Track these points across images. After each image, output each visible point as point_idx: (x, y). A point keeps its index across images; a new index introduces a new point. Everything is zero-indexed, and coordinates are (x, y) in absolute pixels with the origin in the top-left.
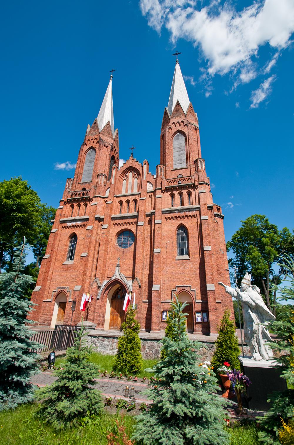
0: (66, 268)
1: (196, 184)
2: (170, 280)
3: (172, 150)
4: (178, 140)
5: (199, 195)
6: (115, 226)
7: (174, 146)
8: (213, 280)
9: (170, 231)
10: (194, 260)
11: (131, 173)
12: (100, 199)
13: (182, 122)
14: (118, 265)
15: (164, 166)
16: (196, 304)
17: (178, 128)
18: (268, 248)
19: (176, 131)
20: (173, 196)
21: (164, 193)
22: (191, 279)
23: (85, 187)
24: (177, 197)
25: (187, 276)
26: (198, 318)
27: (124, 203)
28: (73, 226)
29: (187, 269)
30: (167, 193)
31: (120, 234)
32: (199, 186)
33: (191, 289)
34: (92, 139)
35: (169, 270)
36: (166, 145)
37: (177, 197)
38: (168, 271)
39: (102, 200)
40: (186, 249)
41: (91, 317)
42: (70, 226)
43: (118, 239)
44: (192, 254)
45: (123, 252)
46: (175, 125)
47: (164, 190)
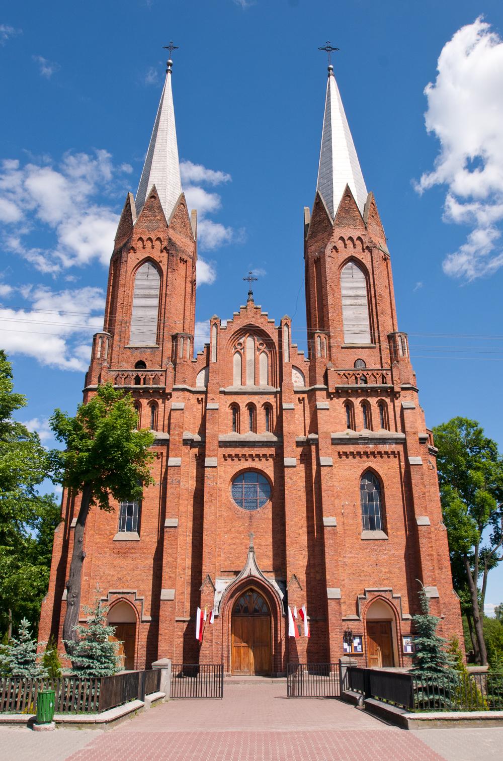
0: (124, 550)
1: (397, 389)
2: (354, 579)
4: (351, 280)
6: (226, 460)
8: (434, 580)
9: (347, 480)
10: (396, 540)
11: (249, 338)
12: (187, 394)
13: (359, 238)
14: (251, 549)
15: (327, 337)
16: (402, 623)
17: (351, 251)
18: (481, 493)
19: (347, 257)
20: (349, 406)
21: (332, 399)
22: (391, 576)
23: (144, 360)
25: (384, 570)
26: (406, 647)
27: (244, 410)
29: (384, 558)
30: (338, 398)
31: (238, 478)
32: (403, 393)
33: (394, 596)
34: (150, 239)
35: (350, 558)
36: (328, 287)
38: (348, 561)
40: (377, 516)
41: (208, 652)
43: (233, 488)
44: (392, 528)
45: (251, 518)
46: (345, 245)
47: (333, 393)
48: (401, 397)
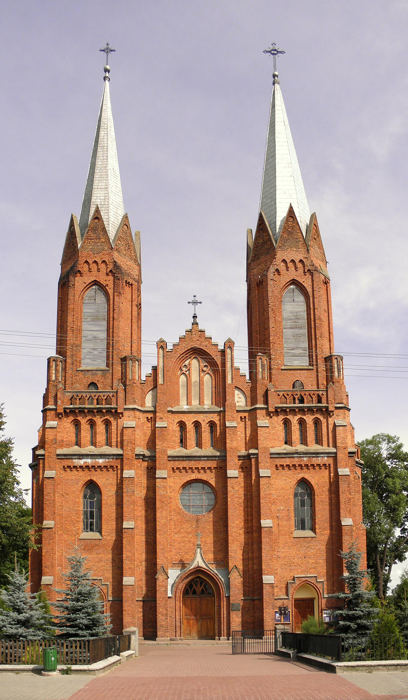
1: (331, 408)
3: (281, 322)
5: (122, 430)
7: (285, 315)
9: (283, 489)
12: (137, 413)
14: (199, 546)
20: (77, 424)
21: (271, 417)
22: (317, 565)
24: (85, 427)
25: (311, 561)
27: (190, 427)
28: (87, 467)
32: (336, 412)
33: (318, 580)
35: (283, 553)
37: (85, 427)
39: (141, 415)
42: (81, 467)
44: (320, 528)
47: (272, 412)
48: (335, 415)
